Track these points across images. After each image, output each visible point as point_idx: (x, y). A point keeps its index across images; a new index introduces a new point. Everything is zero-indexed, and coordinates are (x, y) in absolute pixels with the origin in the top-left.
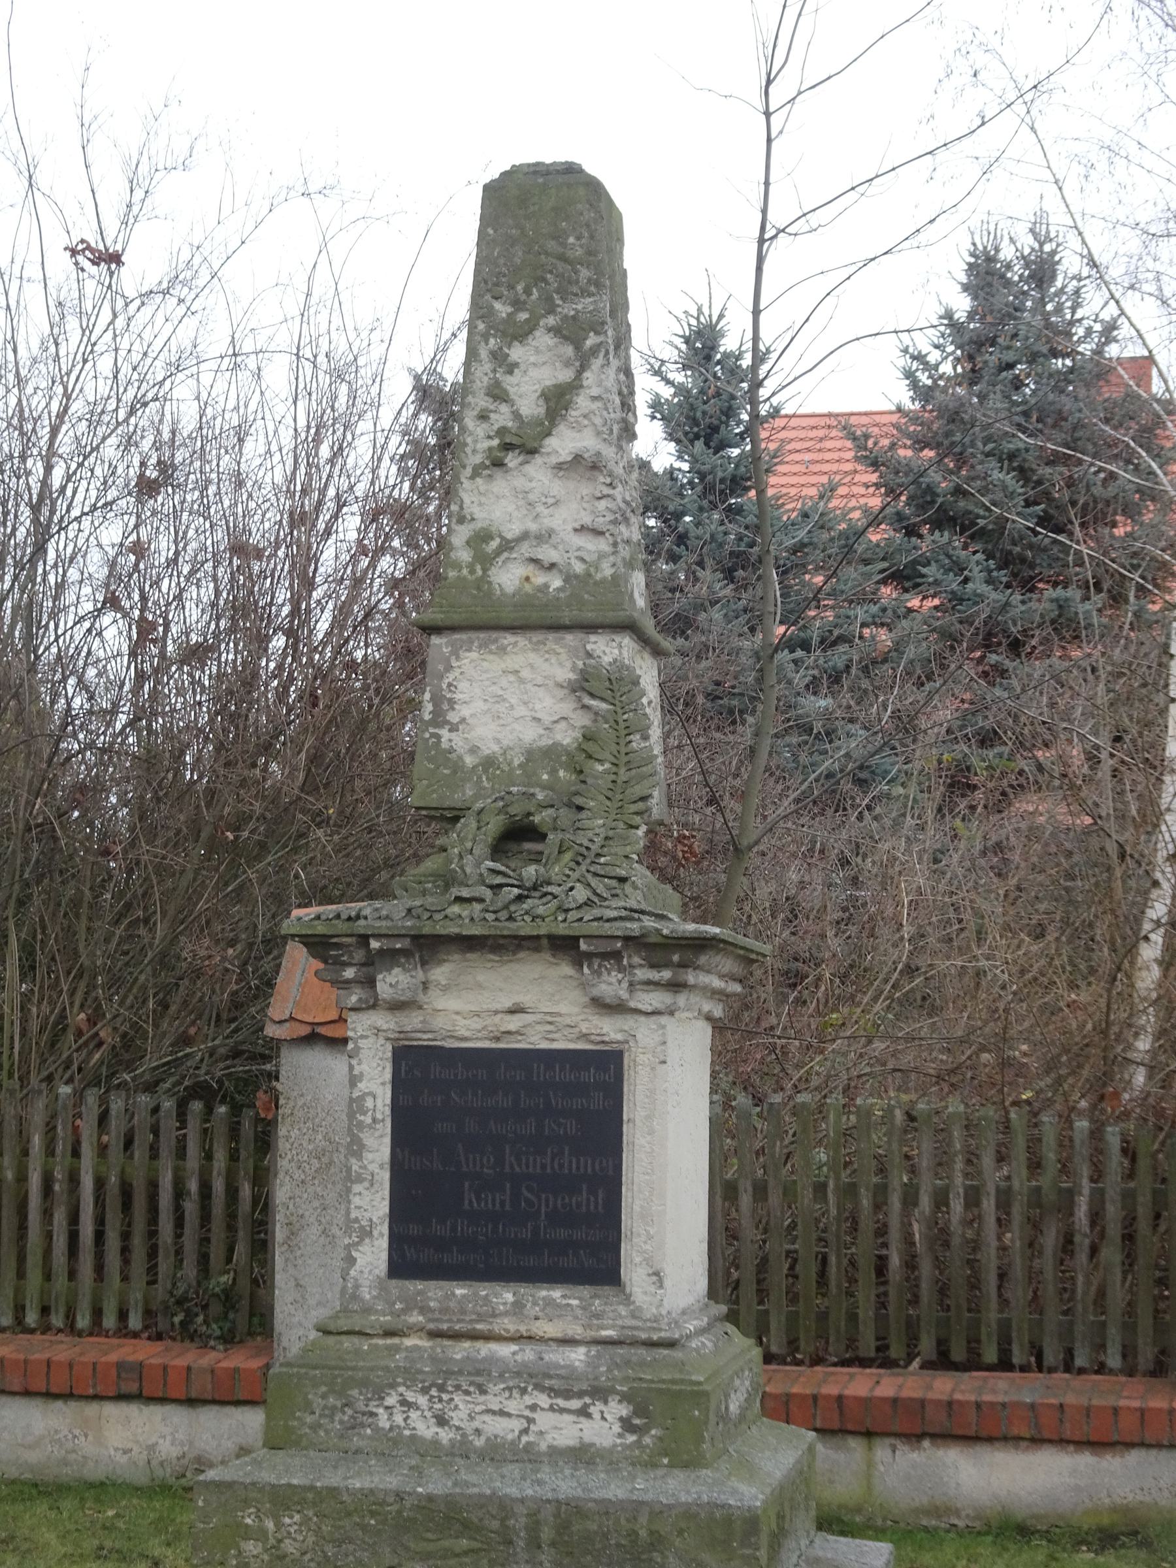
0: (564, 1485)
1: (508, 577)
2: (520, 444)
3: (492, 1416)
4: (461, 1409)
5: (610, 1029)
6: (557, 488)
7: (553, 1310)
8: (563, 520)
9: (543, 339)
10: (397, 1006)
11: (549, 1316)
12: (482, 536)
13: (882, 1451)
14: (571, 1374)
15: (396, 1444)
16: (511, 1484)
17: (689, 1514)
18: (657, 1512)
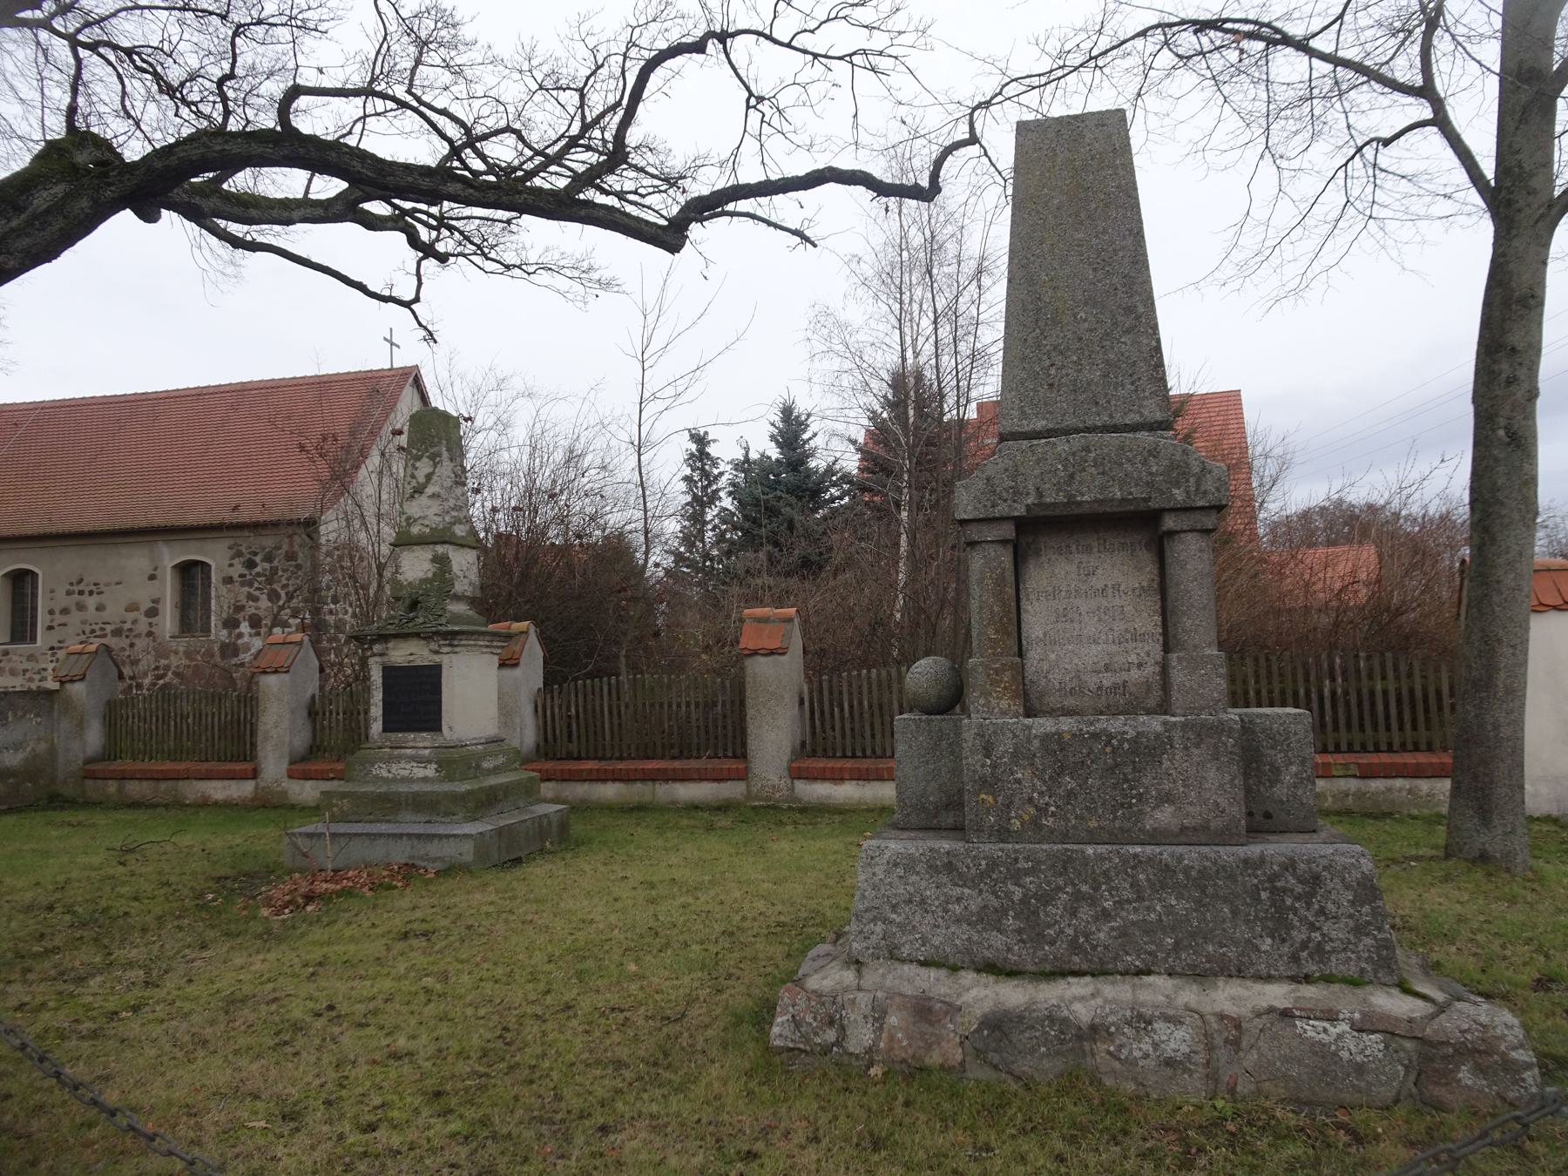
0: (416, 788)
1: (415, 530)
2: (419, 490)
3: (402, 770)
4: (394, 768)
5: (437, 658)
6: (430, 502)
7: (424, 739)
8: (431, 512)
9: (425, 460)
10: (381, 655)
11: (422, 741)
12: (408, 518)
13: (657, 785)
14: (423, 756)
15: (378, 778)
16: (403, 788)
17: (446, 794)
18: (438, 794)
